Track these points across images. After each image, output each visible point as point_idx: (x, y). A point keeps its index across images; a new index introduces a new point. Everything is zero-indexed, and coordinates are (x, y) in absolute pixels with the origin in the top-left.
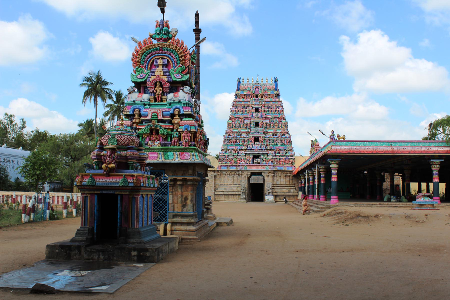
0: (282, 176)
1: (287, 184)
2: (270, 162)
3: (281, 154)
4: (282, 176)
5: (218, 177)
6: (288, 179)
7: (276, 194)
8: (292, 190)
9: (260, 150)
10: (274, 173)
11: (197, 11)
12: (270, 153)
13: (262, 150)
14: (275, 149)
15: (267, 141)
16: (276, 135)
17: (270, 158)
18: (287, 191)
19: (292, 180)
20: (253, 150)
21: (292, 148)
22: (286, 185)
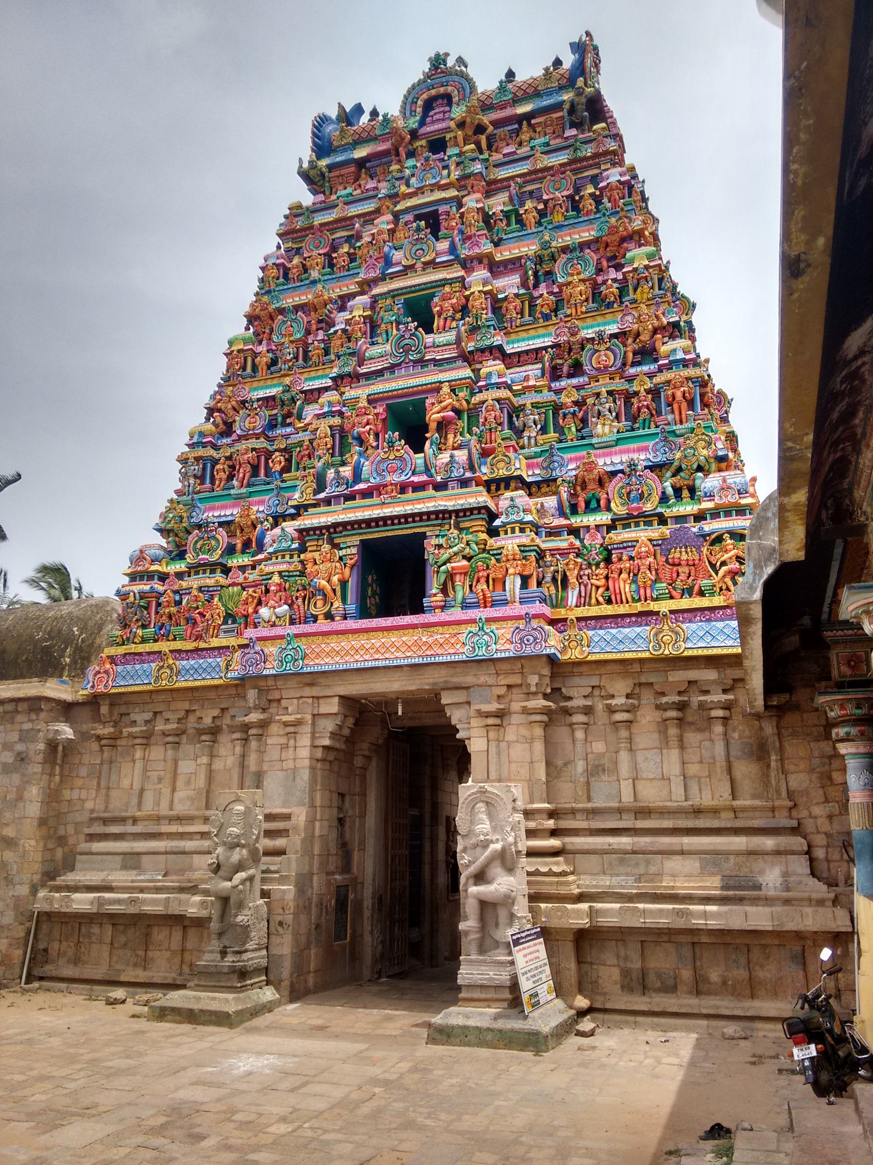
0: (648, 717)
1: (706, 800)
2: (513, 584)
3: (619, 508)
4: (648, 717)
5: (91, 755)
6: (713, 745)
7: (577, 915)
8: (771, 878)
9: (419, 487)
10: (555, 694)
11: (585, 50)
12: (514, 503)
13: (440, 487)
14: (570, 470)
15: (491, 415)
16: (577, 369)
17: (510, 543)
18: (712, 885)
19: (760, 752)
20: (366, 494)
21: (732, 438)
22: (694, 821)
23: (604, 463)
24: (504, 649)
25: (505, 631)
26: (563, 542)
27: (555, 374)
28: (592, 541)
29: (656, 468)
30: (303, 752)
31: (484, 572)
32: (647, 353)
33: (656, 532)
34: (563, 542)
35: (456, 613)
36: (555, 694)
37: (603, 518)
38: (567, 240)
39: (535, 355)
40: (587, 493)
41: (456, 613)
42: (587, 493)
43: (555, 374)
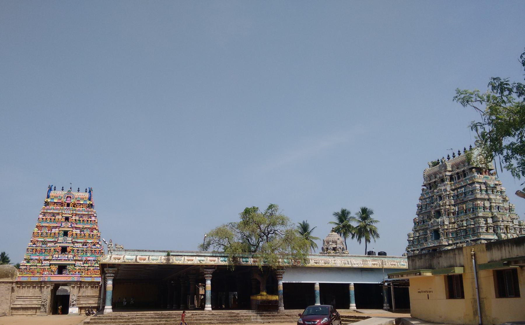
0: (90, 287)
2: (77, 273)
7: (81, 306)
12: (78, 263)
14: (84, 259)
17: (77, 268)
23: (88, 259)
24: (76, 280)
25: (76, 278)
26: (83, 268)
27: (83, 245)
28: (86, 268)
29: (94, 260)
30: (49, 289)
31: (74, 270)
32: (94, 245)
33: (93, 268)
34: (83, 268)
35: (70, 275)
36: (80, 285)
37: (87, 265)
38: (86, 227)
39: (81, 242)
40: (86, 261)
41: (70, 275)
42: (86, 261)
43: (83, 245)
